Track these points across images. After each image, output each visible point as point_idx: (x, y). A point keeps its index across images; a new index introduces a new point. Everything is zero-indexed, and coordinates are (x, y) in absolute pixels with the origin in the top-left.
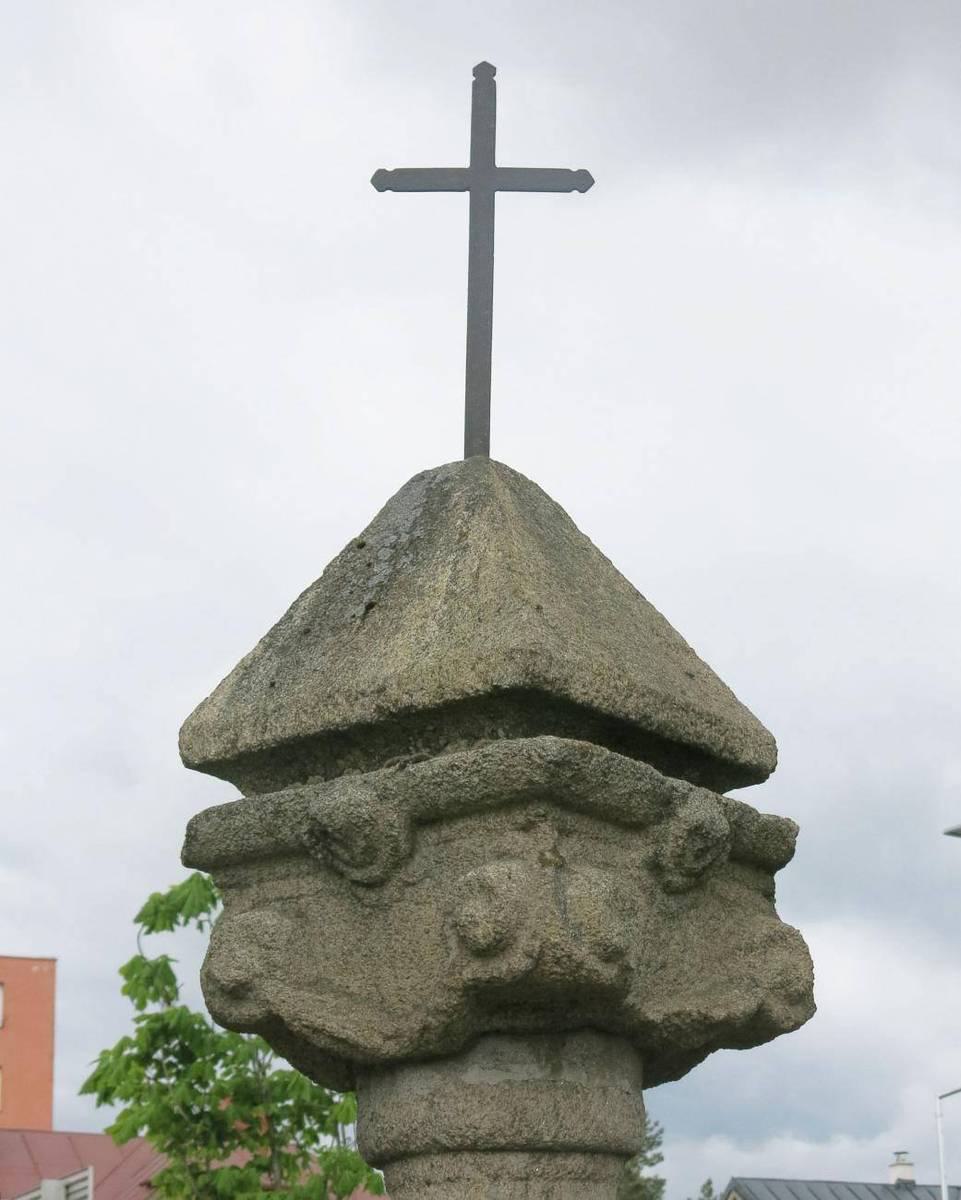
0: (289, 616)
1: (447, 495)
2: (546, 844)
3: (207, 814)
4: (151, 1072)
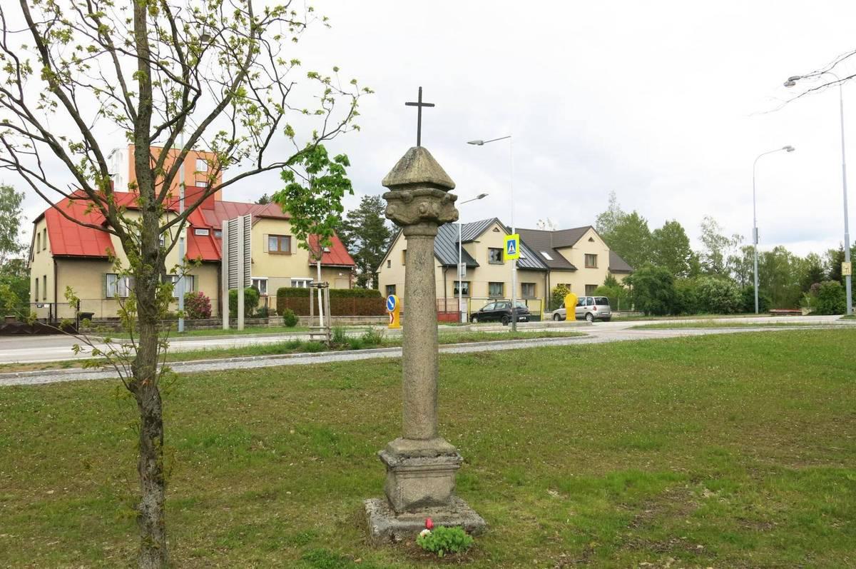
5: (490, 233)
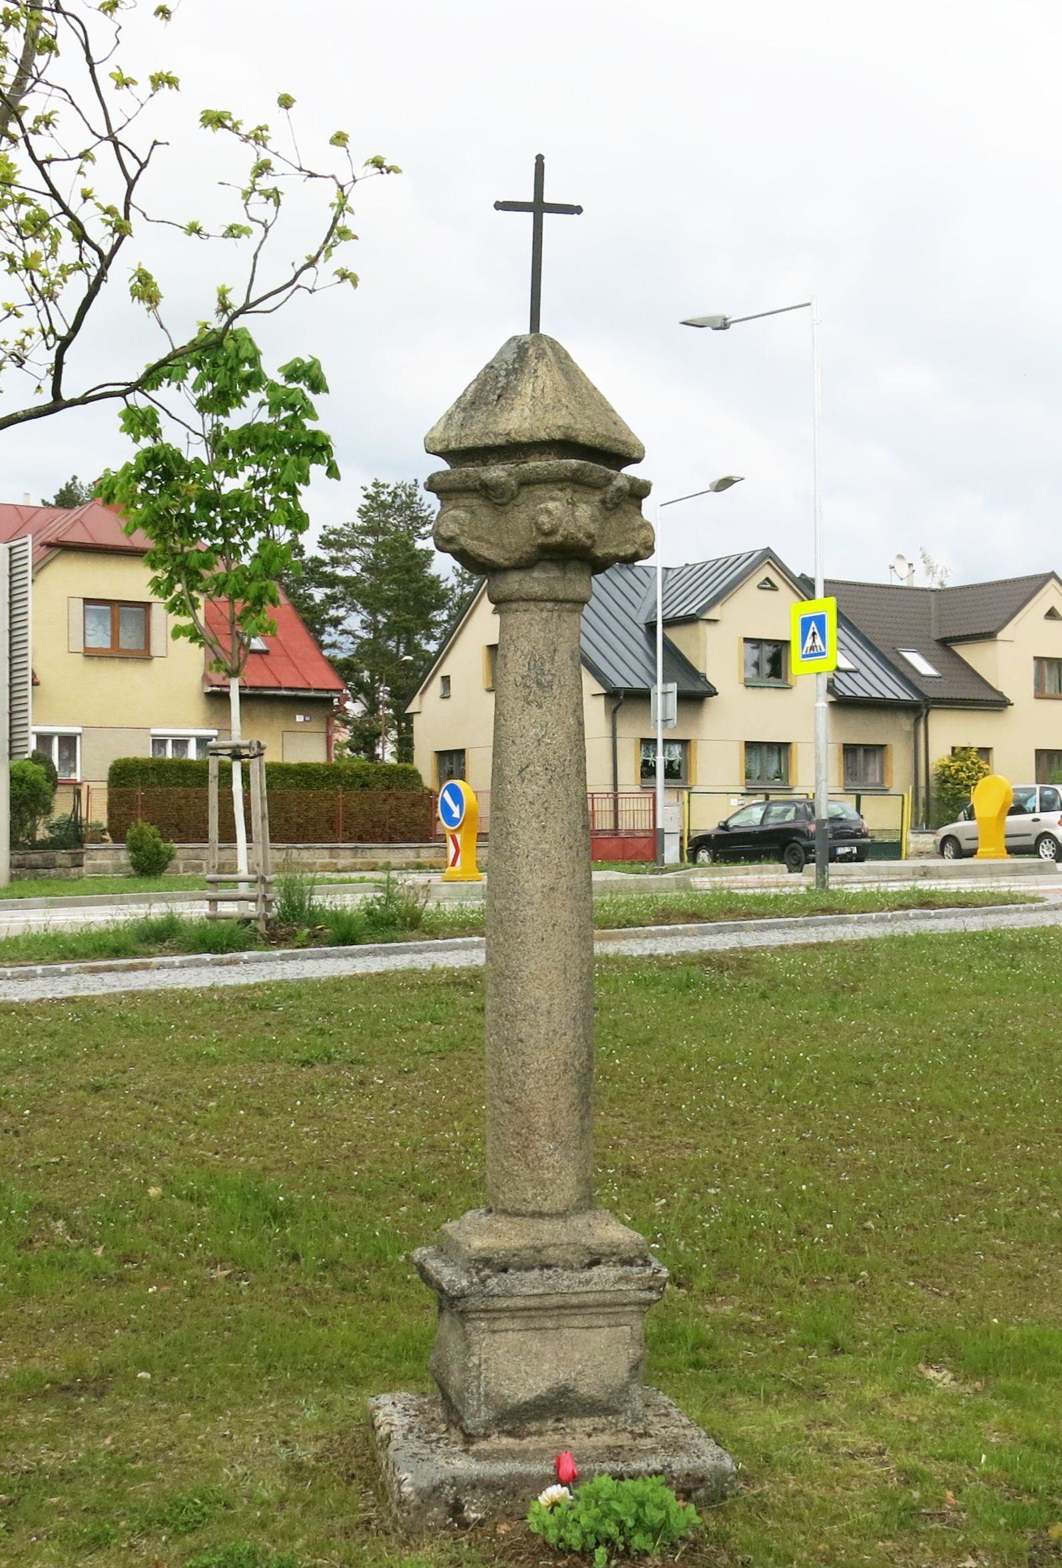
0: (464, 395)
1: (527, 349)
2: (569, 496)
3: (438, 473)
4: (143, 485)
5: (749, 592)
